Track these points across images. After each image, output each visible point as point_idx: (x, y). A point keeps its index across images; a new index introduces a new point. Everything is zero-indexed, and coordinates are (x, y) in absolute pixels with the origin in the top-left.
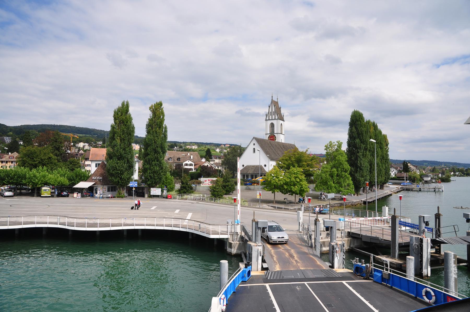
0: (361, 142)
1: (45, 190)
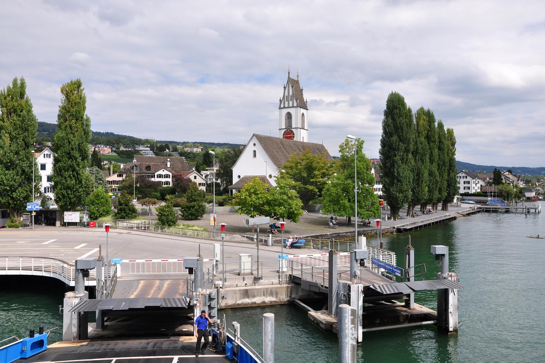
0: (400, 140)
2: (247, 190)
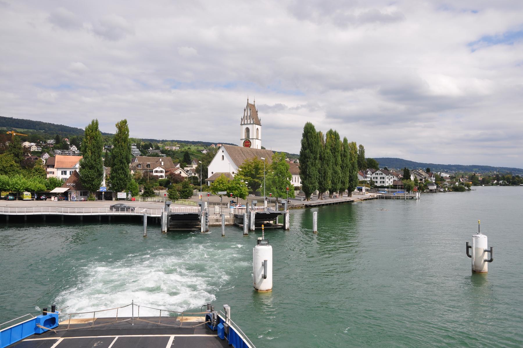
1: (27, 195)
2: (218, 182)
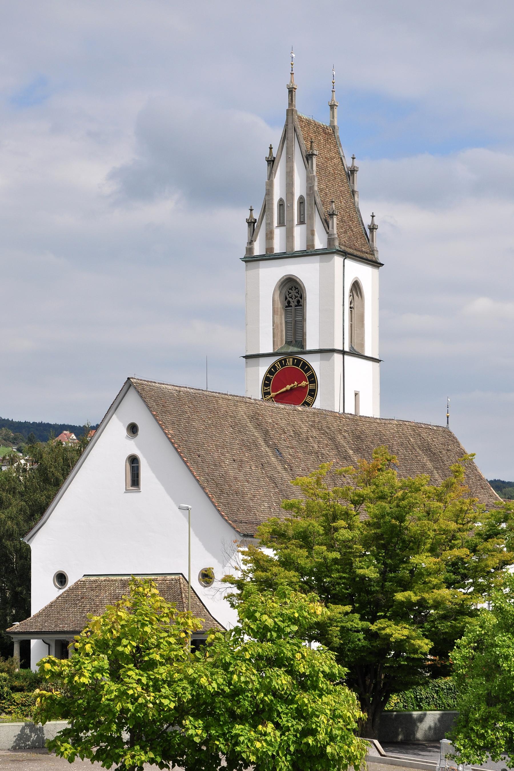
2: (102, 646)
